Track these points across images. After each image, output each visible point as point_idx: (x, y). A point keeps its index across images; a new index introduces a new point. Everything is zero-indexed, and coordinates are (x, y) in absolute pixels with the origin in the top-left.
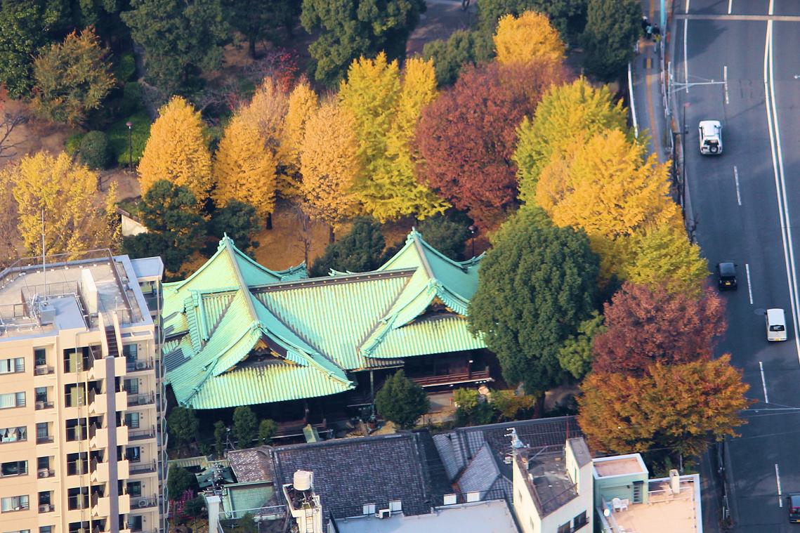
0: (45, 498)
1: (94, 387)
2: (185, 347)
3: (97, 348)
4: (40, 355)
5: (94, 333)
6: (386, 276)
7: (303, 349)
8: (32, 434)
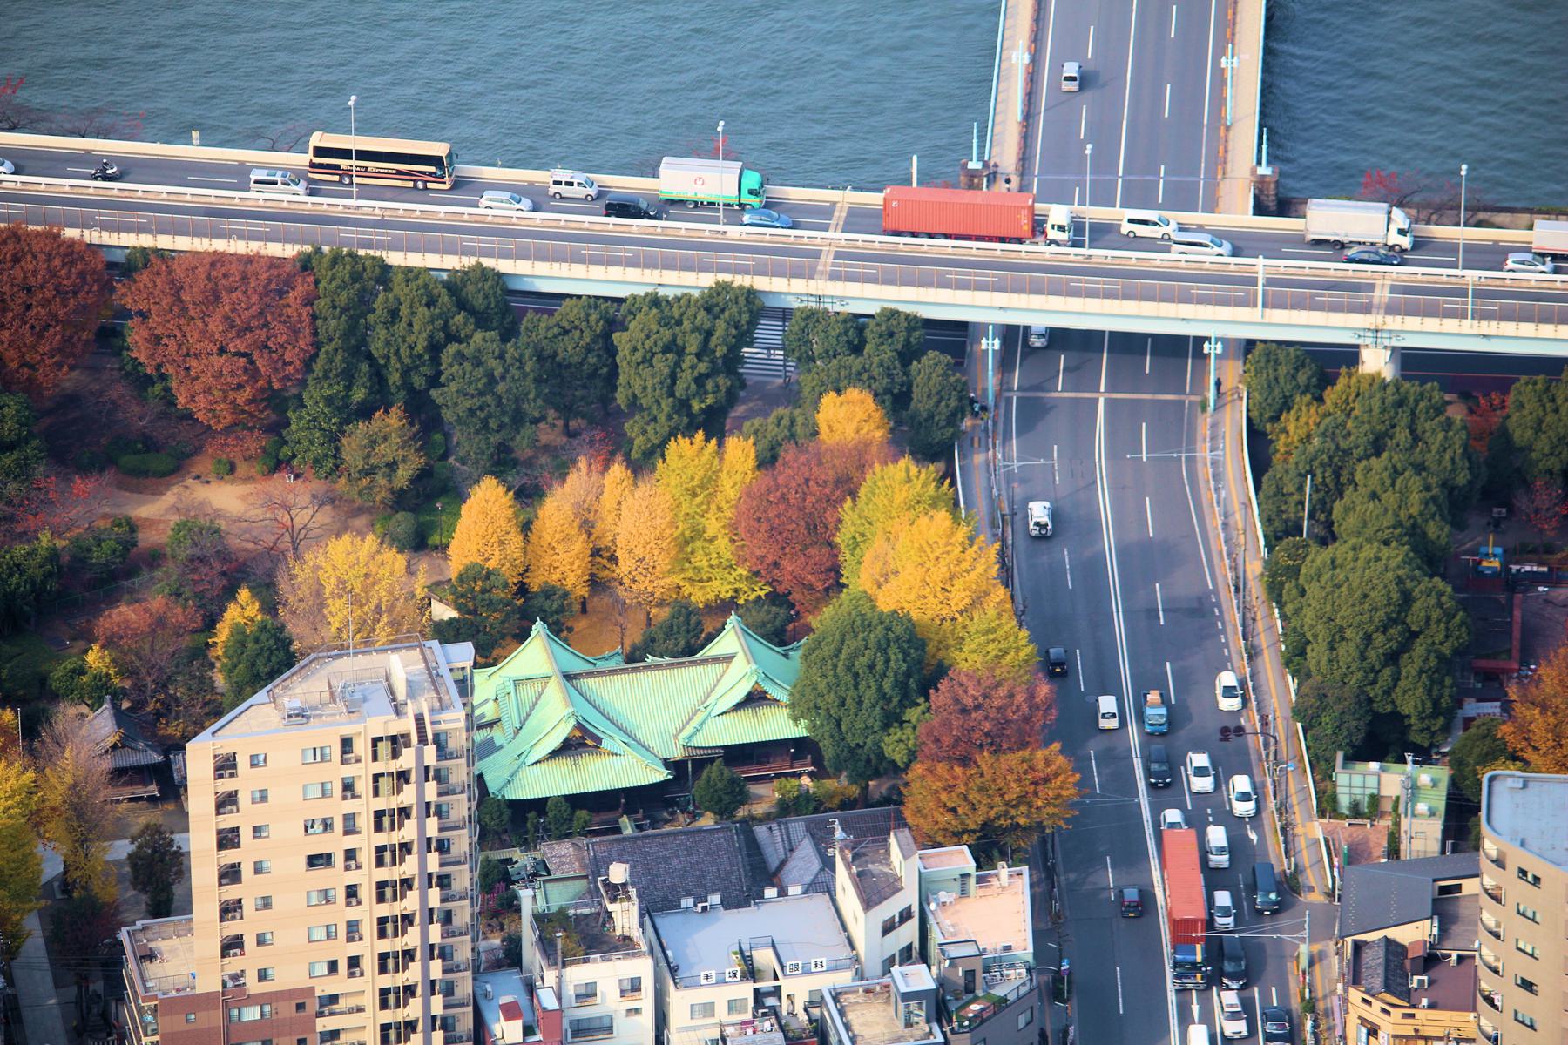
1: (403, 776)
2: (497, 735)
3: (406, 736)
4: (347, 744)
5: (403, 721)
6: (705, 661)
8: (339, 825)
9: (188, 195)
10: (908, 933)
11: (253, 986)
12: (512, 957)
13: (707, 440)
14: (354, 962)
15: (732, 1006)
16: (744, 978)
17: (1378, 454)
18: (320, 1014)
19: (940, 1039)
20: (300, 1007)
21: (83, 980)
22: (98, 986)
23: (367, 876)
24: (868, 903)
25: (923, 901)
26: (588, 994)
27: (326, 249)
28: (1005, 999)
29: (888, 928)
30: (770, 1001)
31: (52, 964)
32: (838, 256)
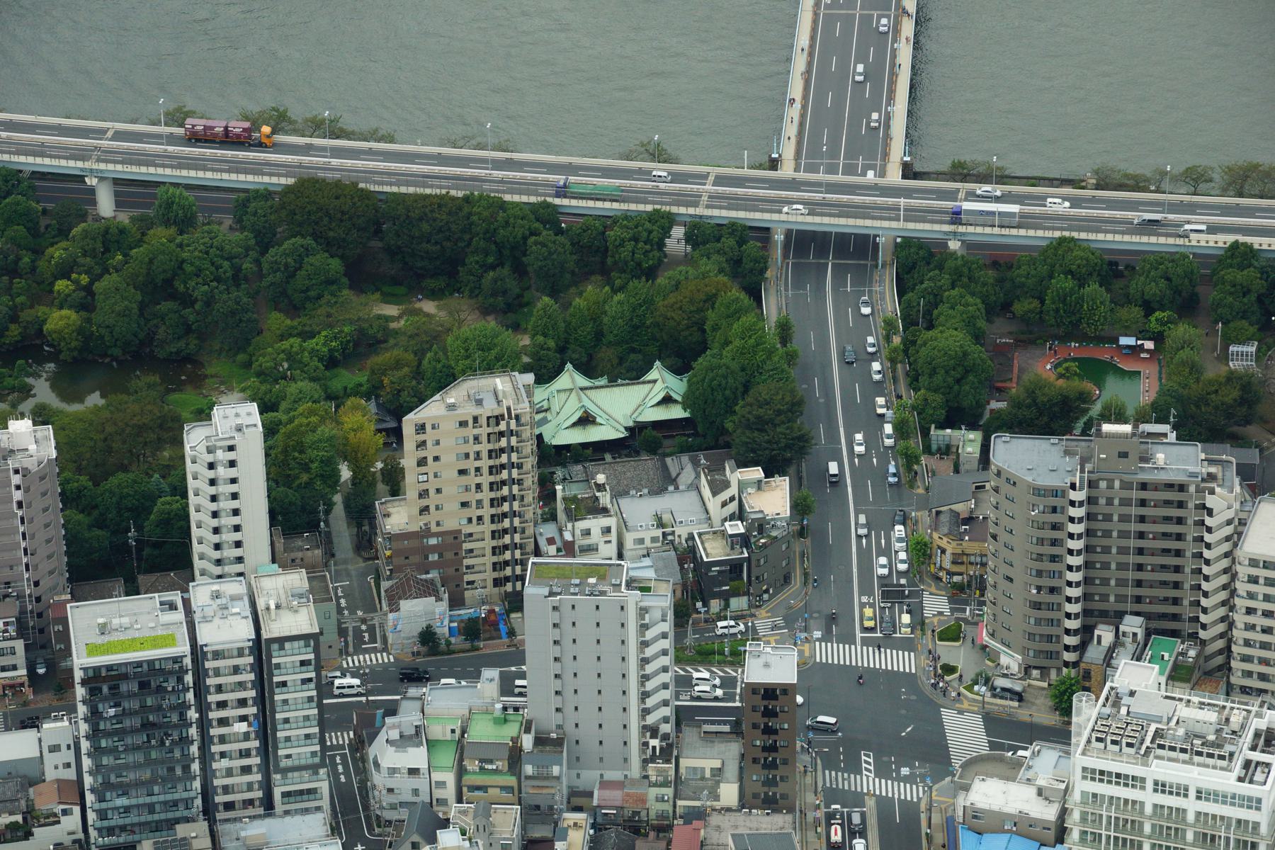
0: (478, 486)
1: (501, 434)
2: (549, 416)
3: (502, 416)
4: (476, 419)
5: (197, 503)
6: (644, 383)
7: (605, 416)
8: (472, 456)
9: (415, 168)
10: (733, 507)
11: (434, 529)
12: (552, 517)
13: (647, 281)
14: (480, 518)
15: (654, 540)
16: (658, 527)
17: (953, 288)
18: (465, 542)
19: (746, 555)
20: (456, 538)
21: (359, 526)
22: (366, 528)
23: (486, 479)
24: (714, 494)
25: (740, 492)
26: (587, 533)
27: (476, 193)
28: (776, 537)
29: (724, 504)
30: (670, 538)
31: (347, 516)
32: (709, 197)
